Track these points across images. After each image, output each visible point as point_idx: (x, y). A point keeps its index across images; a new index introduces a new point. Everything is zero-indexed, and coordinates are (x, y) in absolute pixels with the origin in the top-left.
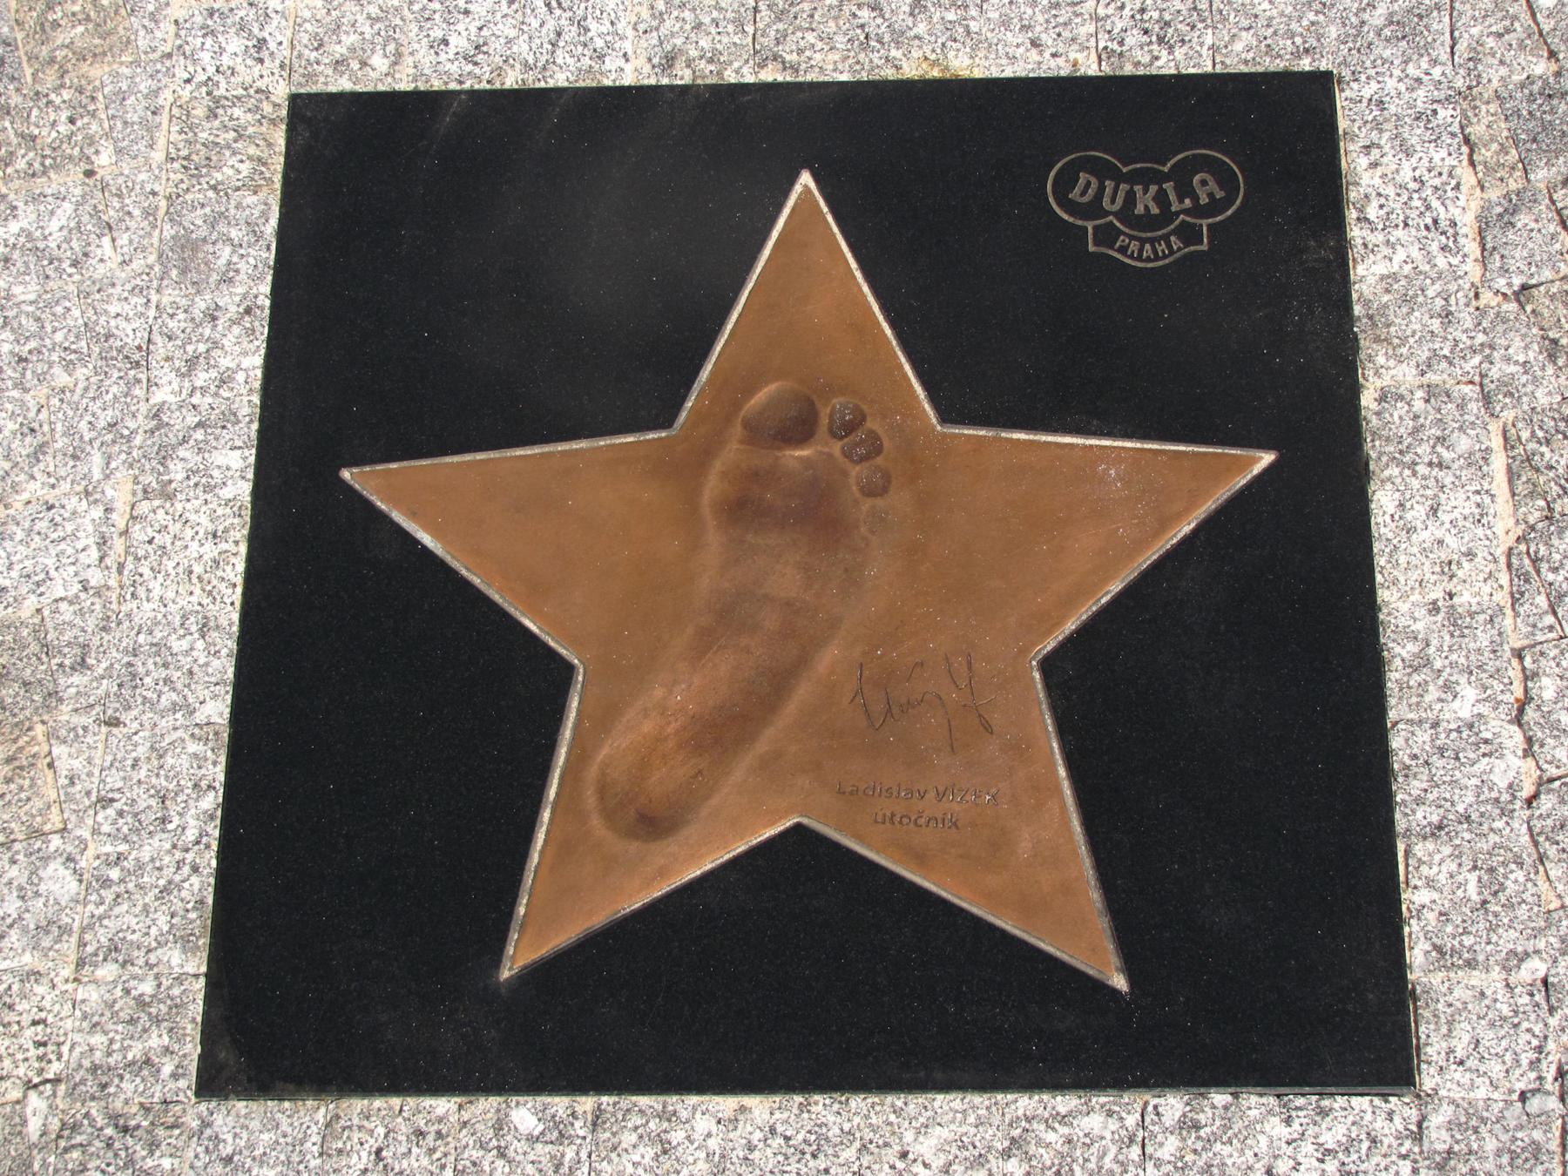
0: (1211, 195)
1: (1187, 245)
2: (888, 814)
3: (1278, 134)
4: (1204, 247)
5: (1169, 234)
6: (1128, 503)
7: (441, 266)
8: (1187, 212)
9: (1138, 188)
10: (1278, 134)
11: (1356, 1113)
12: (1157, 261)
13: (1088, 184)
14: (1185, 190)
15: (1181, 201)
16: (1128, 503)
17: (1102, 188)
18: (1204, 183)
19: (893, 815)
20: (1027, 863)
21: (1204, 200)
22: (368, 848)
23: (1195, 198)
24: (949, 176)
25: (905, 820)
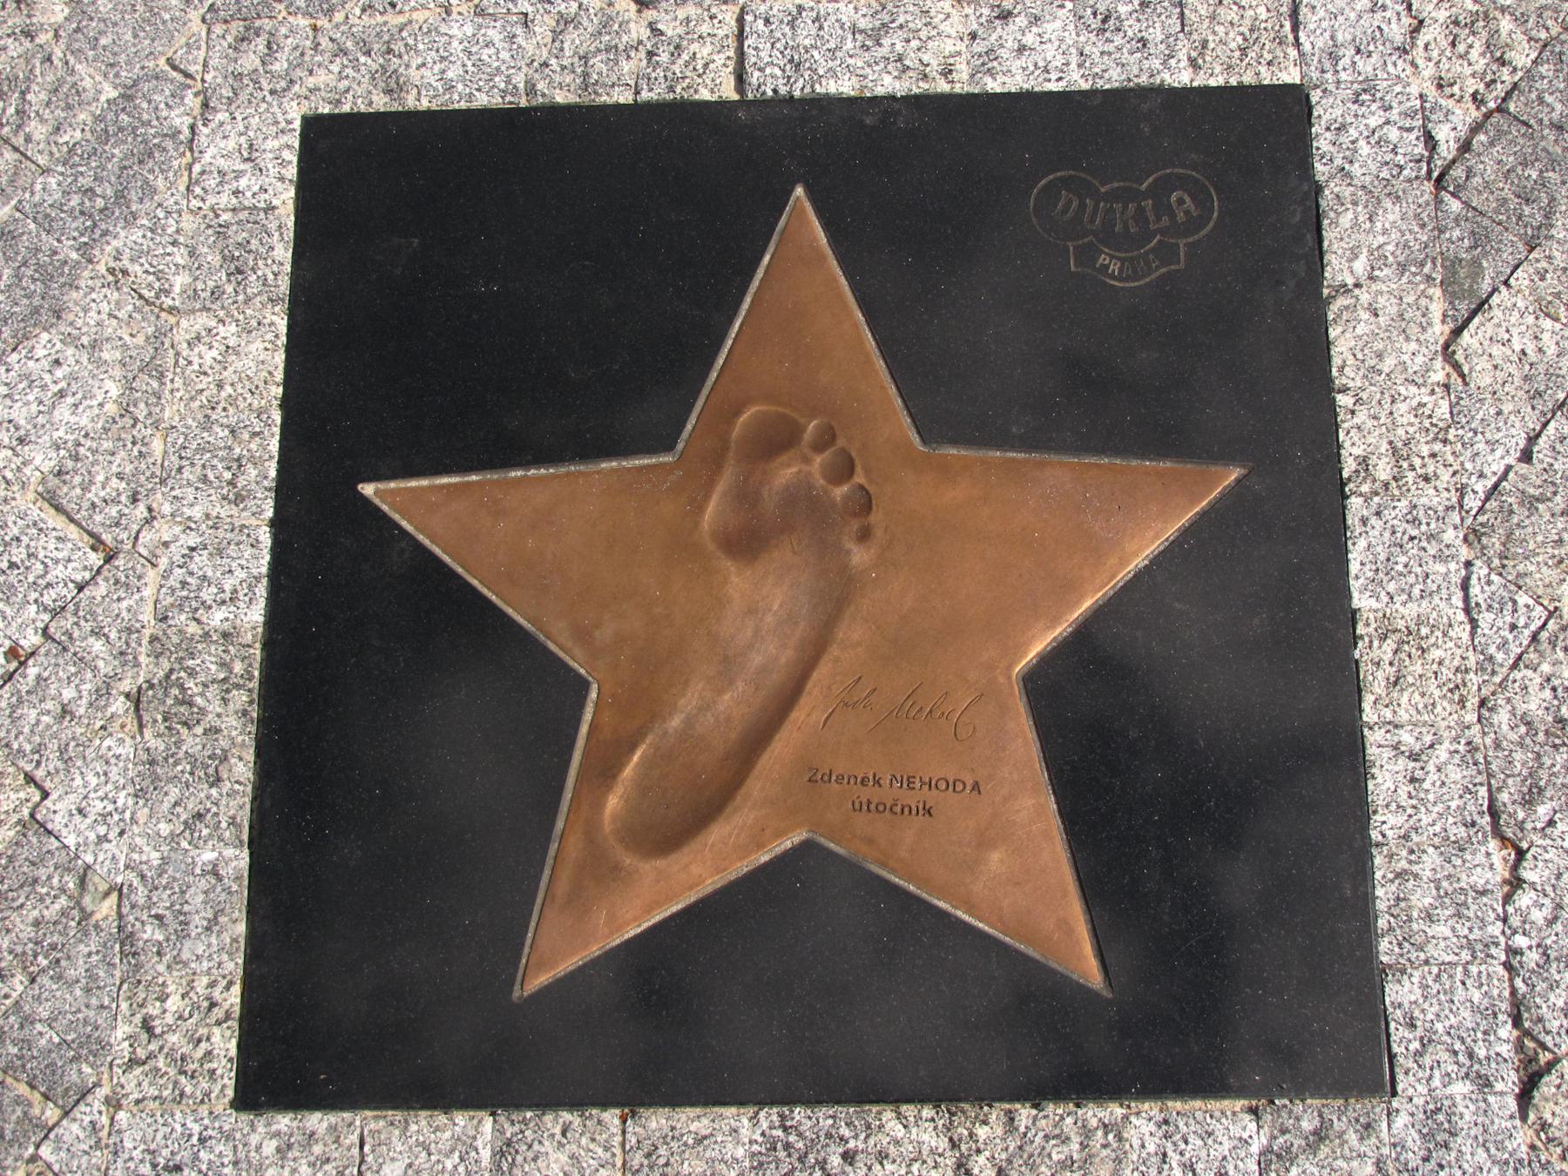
0: (1187, 213)
1: (1163, 265)
2: (864, 801)
3: (1252, 145)
4: (1182, 265)
5: (1147, 253)
6: (1119, 530)
7: (478, 288)
8: (1162, 232)
9: (1118, 206)
10: (1252, 145)
11: (462, 64)
12: (1133, 272)
13: (1070, 202)
14: (1163, 208)
15: (1159, 219)
16: (1119, 530)
17: (1082, 206)
18: (1181, 201)
19: (869, 803)
20: (1011, 868)
21: (1181, 217)
22: (387, 833)
23: (1172, 215)
24: (930, 180)
25: (881, 808)
